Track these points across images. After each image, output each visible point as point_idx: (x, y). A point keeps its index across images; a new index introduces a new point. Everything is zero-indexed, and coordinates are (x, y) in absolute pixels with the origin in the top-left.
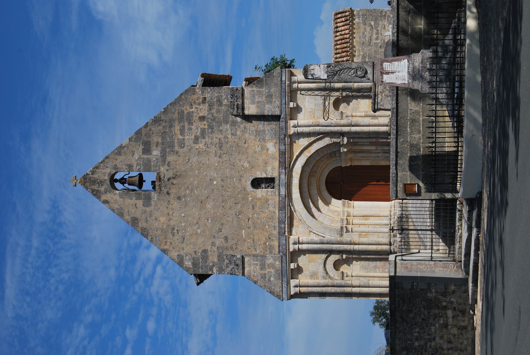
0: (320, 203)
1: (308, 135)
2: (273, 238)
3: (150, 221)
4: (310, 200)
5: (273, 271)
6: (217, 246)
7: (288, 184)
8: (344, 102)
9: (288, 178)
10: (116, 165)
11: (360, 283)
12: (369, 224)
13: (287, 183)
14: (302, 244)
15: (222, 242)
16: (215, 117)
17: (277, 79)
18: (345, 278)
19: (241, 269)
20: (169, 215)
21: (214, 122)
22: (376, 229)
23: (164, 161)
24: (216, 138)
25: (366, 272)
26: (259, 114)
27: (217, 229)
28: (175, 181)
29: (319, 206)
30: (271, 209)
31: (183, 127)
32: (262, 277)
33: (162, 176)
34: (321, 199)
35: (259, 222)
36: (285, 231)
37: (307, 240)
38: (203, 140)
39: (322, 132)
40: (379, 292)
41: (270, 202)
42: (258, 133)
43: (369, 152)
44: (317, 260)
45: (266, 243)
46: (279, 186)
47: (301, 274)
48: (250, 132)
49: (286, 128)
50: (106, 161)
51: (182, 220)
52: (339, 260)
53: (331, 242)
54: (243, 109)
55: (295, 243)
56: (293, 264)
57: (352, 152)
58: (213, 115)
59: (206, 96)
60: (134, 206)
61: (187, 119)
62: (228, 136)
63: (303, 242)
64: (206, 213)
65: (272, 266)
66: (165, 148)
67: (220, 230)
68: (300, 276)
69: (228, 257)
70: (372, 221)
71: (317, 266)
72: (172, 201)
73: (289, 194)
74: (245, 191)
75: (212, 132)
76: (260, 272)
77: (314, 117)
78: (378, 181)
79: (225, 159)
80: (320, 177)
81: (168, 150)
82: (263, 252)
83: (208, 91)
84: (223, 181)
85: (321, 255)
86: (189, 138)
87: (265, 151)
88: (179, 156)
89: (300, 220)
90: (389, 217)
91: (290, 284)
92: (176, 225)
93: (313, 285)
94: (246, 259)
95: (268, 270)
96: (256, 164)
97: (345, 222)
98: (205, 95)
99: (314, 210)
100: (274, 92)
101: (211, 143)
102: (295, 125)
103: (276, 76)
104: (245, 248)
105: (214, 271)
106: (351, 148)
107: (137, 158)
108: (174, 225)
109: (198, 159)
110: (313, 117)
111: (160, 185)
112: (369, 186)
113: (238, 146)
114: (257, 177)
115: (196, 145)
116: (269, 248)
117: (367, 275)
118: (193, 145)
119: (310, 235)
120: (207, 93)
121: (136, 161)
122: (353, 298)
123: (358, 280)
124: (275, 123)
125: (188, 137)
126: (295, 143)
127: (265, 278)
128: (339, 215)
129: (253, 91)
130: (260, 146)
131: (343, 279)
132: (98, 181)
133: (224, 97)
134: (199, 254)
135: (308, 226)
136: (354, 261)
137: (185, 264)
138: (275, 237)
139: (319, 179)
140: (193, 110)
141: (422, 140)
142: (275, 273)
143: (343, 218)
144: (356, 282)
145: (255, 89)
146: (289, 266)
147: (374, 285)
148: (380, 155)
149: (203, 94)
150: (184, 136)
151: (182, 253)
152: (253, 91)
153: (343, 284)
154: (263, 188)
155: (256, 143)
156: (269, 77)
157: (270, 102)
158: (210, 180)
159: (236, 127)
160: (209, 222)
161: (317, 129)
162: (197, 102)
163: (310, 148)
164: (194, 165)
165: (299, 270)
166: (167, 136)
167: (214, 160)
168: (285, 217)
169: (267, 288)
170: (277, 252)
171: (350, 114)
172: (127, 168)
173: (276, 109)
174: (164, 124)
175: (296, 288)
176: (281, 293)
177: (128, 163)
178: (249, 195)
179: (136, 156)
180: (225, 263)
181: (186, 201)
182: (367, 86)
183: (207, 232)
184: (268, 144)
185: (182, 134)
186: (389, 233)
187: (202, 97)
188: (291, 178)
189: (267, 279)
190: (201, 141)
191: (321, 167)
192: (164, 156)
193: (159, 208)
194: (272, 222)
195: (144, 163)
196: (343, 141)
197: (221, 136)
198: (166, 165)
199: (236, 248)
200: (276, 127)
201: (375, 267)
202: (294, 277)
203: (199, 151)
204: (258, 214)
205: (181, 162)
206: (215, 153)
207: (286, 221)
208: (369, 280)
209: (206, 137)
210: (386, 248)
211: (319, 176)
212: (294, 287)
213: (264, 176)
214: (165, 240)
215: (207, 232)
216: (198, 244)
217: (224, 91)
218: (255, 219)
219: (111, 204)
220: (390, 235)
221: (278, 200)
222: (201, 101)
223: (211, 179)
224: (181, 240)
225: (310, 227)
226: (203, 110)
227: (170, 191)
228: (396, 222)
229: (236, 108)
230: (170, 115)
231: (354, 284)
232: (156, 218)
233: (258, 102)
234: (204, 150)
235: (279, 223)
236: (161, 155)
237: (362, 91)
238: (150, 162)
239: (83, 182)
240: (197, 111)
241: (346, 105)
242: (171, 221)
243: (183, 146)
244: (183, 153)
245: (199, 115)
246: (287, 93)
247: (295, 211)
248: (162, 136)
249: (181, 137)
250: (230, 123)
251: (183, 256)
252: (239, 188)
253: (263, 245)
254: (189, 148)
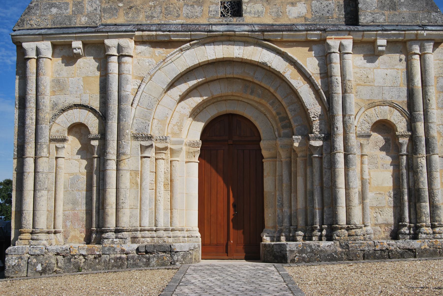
0: (196, 101)
2: (130, 15)
4: (201, 80)
5: (69, 11)
9: (244, 36)
11: (43, 173)
12: (158, 190)
13: (235, 36)
17: (425, 18)
18: (53, 146)
22: (148, 203)
25: (65, 185)
29: (190, 99)
30: (185, 10)
34: (204, 102)
36: (143, 31)
37: (125, 72)
40: (24, 209)
41: (198, 9)
43: (292, 189)
44: (88, 91)
46: (227, 24)
47: (62, 63)
52: (89, 133)
53: (121, 117)
55: (120, 48)
56: (81, 46)
63: (123, 65)
68: (59, 60)
71: (76, 92)
77: (358, 85)
78: (234, 206)
80: (241, 101)
85: (99, 100)
89: (164, 60)
90: (171, 228)
91: (43, 40)
93: (40, 83)
99: (183, 87)
100: (400, 14)
102: (344, 49)
103: (430, 17)
106: (299, 155)
110: (359, 82)
116: (113, 7)
117: (58, 186)
122: (16, 160)
123: (49, 169)
124: (341, 16)
128: (174, 134)
131: (52, 140)
135: (153, 75)
136: (86, 163)
138: (133, 18)
139: (238, 100)
141: (73, 245)
143: (168, 141)
144: (43, 164)
146: (77, 39)
147: (38, 200)
148: (286, 209)
153: (40, 141)
161: (338, 88)
163: (300, 77)
168: (169, 31)
170: (104, 21)
171: (365, 151)
176: (29, 26)
184: (304, 5)
188: (234, 60)
191: (260, 103)
194: (161, 12)
196: (316, 138)
201: (75, 203)
202: (57, 51)
207: (162, 33)
208: (48, 191)
210: (111, 223)
211: (243, 100)
212: (37, 48)
220: (136, 231)
228: (161, 242)
235: (159, 24)
237: (411, 174)
241: (381, 146)
246: (403, 32)
247: (181, 50)
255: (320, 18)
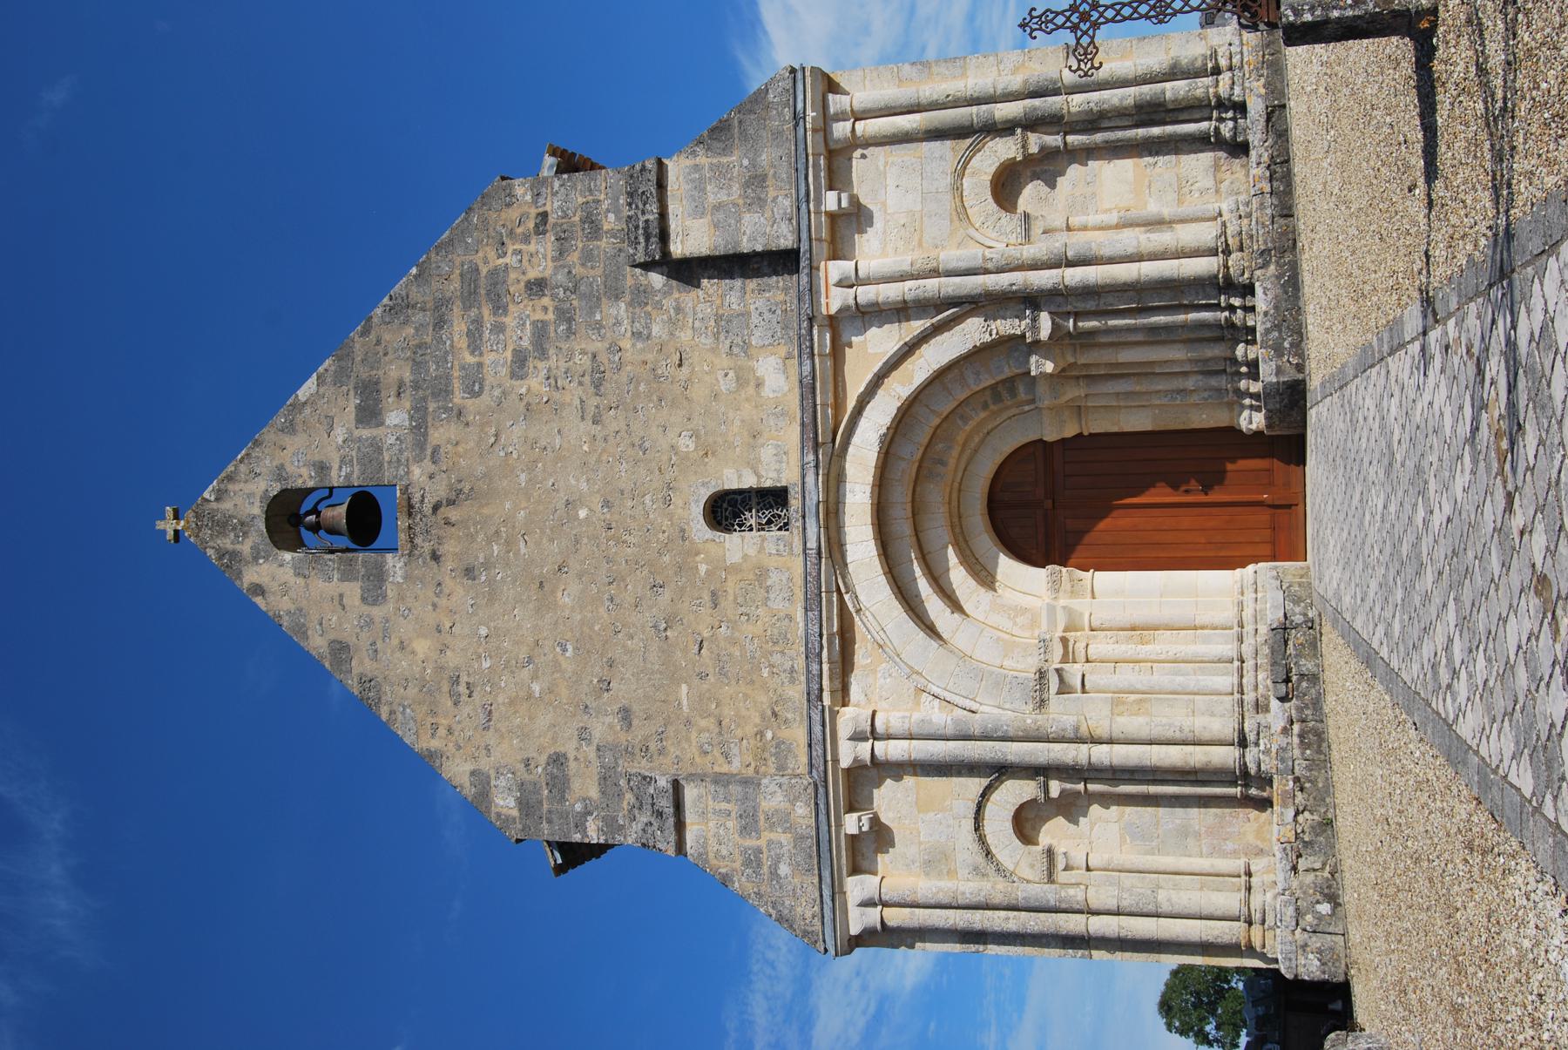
0: (958, 576)
1: (901, 311)
2: (789, 716)
3: (385, 653)
5: (785, 839)
6: (595, 742)
7: (832, 508)
8: (1035, 176)
10: (281, 467)
11: (1119, 898)
12: (1153, 657)
13: (826, 502)
14: (889, 739)
15: (611, 726)
16: (578, 277)
17: (780, 114)
18: (1062, 876)
19: (672, 829)
20: (440, 632)
21: (573, 296)
23: (421, 445)
24: (583, 352)
26: (721, 251)
27: (595, 680)
28: (453, 514)
30: (778, 604)
31: (478, 322)
32: (747, 863)
33: (416, 498)
35: (738, 653)
36: (821, 690)
37: (906, 726)
38: (541, 365)
39: (948, 298)
41: (774, 579)
42: (724, 323)
43: (1145, 372)
45: (761, 734)
46: (804, 517)
48: (697, 324)
49: (811, 290)
50: (253, 455)
51: (481, 650)
52: (1033, 801)
53: (999, 734)
54: (664, 237)
55: (857, 737)
57: (1078, 378)
58: (570, 272)
59: (548, 208)
60: (336, 602)
61: (488, 293)
62: (622, 344)
64: (556, 623)
65: (782, 820)
66: (424, 399)
67: (606, 685)
69: (632, 783)
70: (1164, 645)
71: (949, 826)
72: (449, 583)
73: (834, 547)
74: (683, 540)
75: (570, 332)
76: (741, 841)
77: (920, 244)
79: (614, 426)
80: (960, 484)
81: (432, 406)
82: (753, 765)
83: (552, 188)
84: (608, 507)
86: (496, 360)
87: (751, 390)
88: (467, 424)
89: (881, 646)
92: (464, 668)
94: (690, 793)
95: (767, 835)
96: (720, 440)
97: (1058, 651)
98: (545, 204)
101: (566, 373)
102: (847, 278)
104: (692, 751)
105: (589, 834)
106: (1072, 360)
107: (340, 440)
108: (457, 669)
109: (525, 430)
110: (915, 243)
111: (410, 528)
112: (1115, 513)
113: (657, 377)
114: (726, 487)
115: (519, 382)
116: (773, 750)
117: (1148, 866)
118: (508, 383)
119: (918, 704)
120: (549, 195)
121: (339, 449)
124: (781, 284)
125: (492, 356)
126: (850, 346)
127: (760, 865)
128: (1034, 623)
129: (697, 168)
130: (731, 374)
131: (1051, 878)
132: (235, 521)
133: (604, 207)
134: (540, 769)
135: (911, 668)
137: (496, 805)
139: (960, 491)
140: (507, 260)
142: (795, 847)
143: (1048, 637)
144: (1102, 896)
145: (703, 159)
146: (839, 825)
148: (1190, 383)
149: (537, 202)
150: (481, 354)
151: (485, 764)
152: (697, 168)
154: (751, 530)
155: (717, 361)
156: (751, 111)
157: (758, 203)
158: (568, 503)
159: (649, 308)
160: (568, 654)
162: (519, 230)
163: (908, 365)
164: (515, 455)
165: (880, 836)
166: (427, 358)
167: (578, 431)
168: (821, 636)
169: (766, 904)
170: (803, 769)
171: (1059, 222)
172: (313, 474)
173: (779, 227)
174: (418, 317)
175: (870, 910)
176: (817, 922)
177: (317, 458)
178: (697, 554)
179: (339, 434)
180: (625, 803)
181: (490, 582)
182: (1121, 100)
183: (564, 692)
184: (760, 362)
185: (475, 347)
186: (1237, 696)
187: (533, 212)
189: (765, 869)
190: (535, 367)
192: (420, 427)
193: (410, 610)
194: (782, 652)
195: (361, 455)
196: (1034, 327)
197: (598, 346)
198: (428, 457)
199: (661, 752)
200: (788, 299)
201: (1184, 832)
203: (528, 404)
204: (733, 625)
205: (472, 444)
206: (579, 407)
208: (1159, 887)
209: (552, 351)
213: (749, 481)
214: (430, 720)
215: (564, 692)
216: (537, 734)
217: (604, 185)
218: (722, 644)
219: (273, 598)
221: (800, 570)
222: (531, 225)
223: (571, 500)
224: (482, 718)
225: (917, 673)
226: (540, 258)
227: (441, 547)
228: (1266, 650)
229: (642, 239)
230: (435, 285)
231: (1095, 904)
232: (402, 642)
233: (718, 207)
234: (545, 399)
235: (807, 658)
236: (411, 424)
238: (379, 450)
239: (194, 526)
240: (521, 261)
242: (448, 653)
243: (477, 388)
244: (479, 413)
245: (525, 278)
246: (811, 158)
247: (858, 611)
248: (414, 360)
249: (470, 359)
250: (628, 298)
251: (489, 777)
252: (664, 532)
253: (752, 742)
254: (496, 394)
255: (785, 328)
